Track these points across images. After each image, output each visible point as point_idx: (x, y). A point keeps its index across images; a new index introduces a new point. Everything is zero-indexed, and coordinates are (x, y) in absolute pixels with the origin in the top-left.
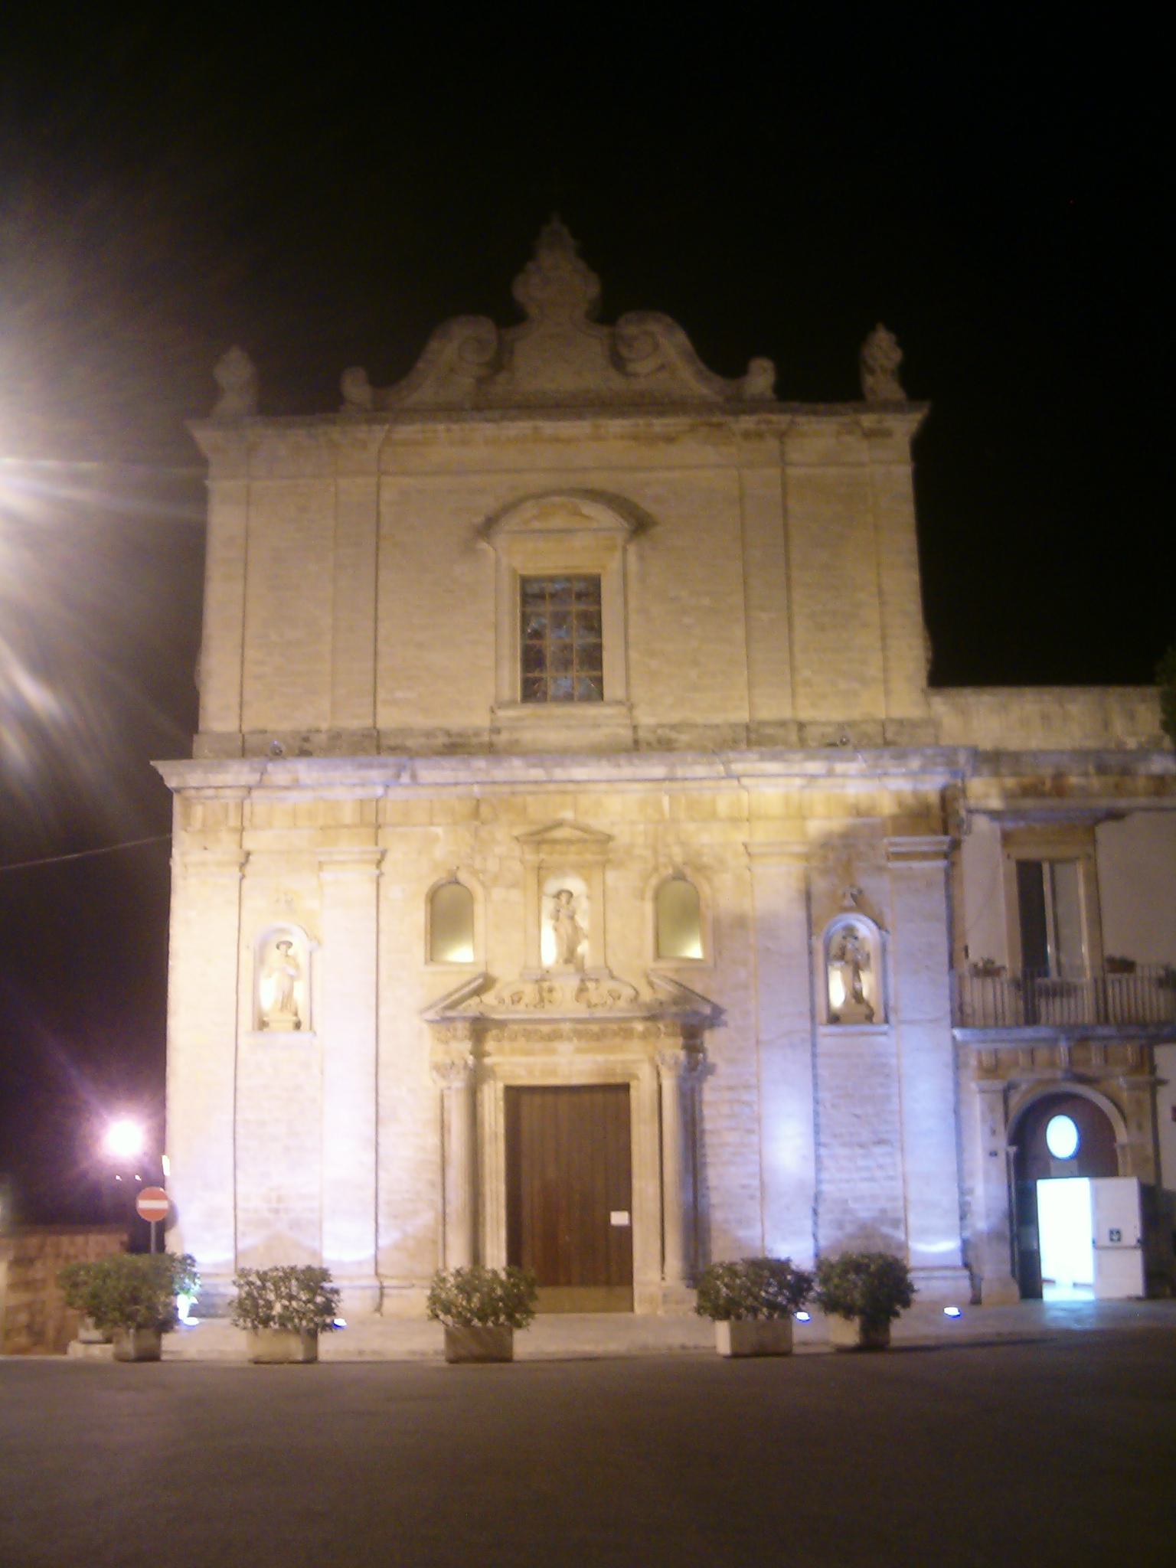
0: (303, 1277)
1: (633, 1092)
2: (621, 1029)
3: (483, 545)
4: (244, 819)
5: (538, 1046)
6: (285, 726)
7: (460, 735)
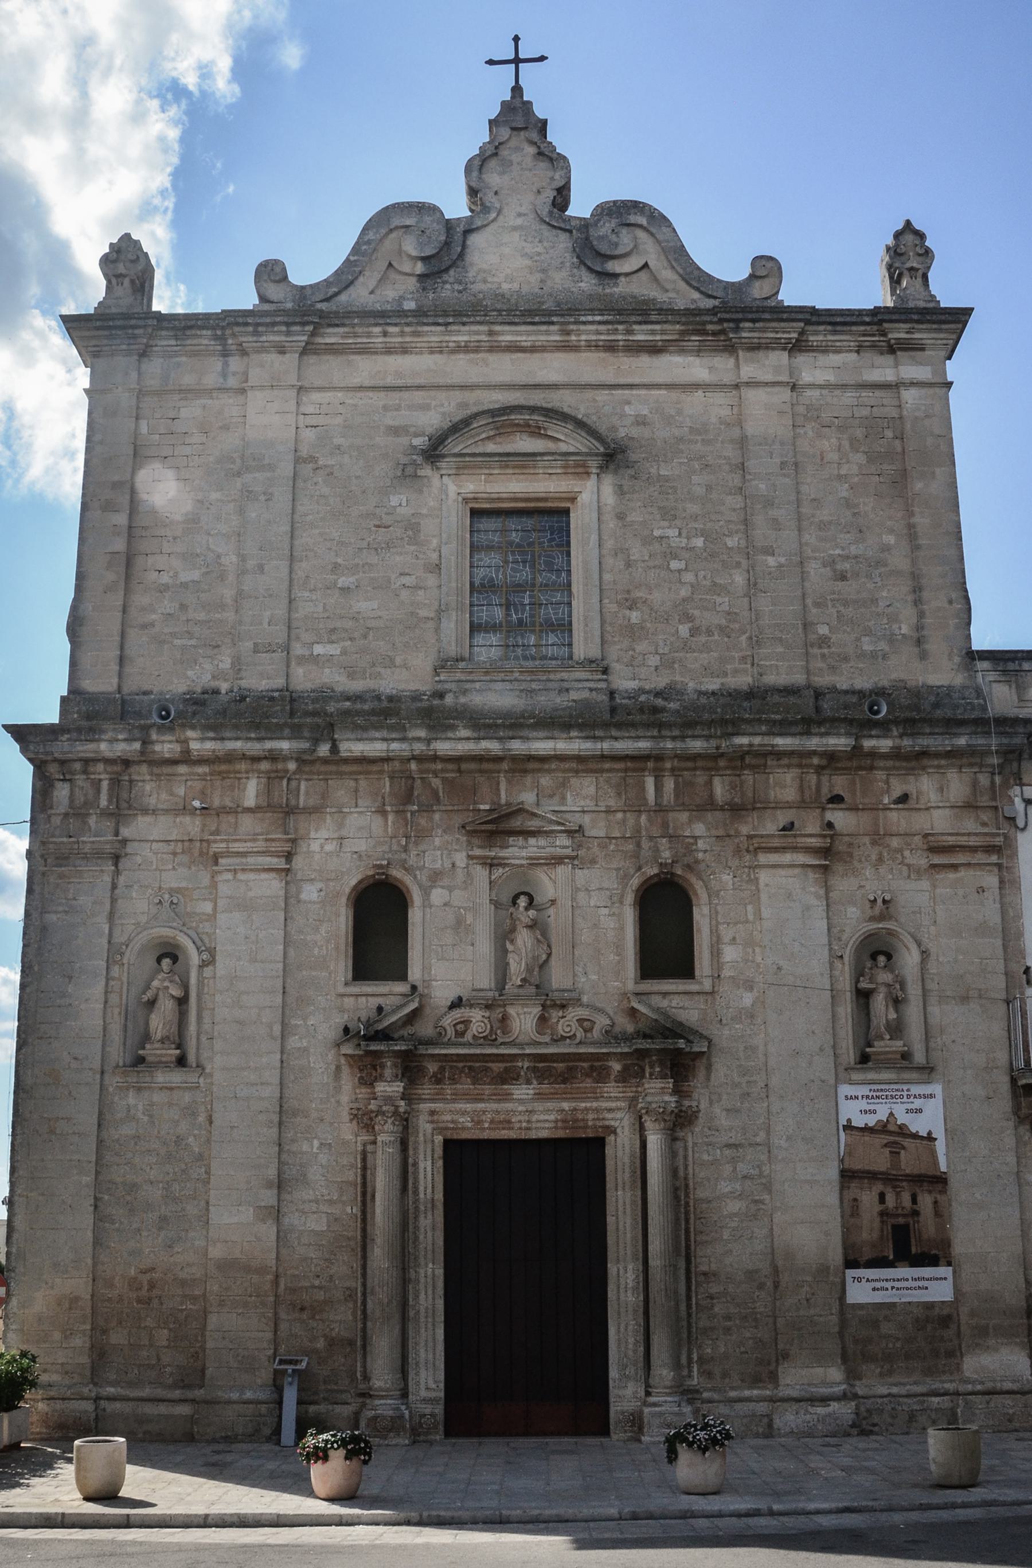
0: (717, 782)
1: (609, 1151)
2: (592, 1067)
3: (427, 471)
4: (580, 1516)
5: (488, 1089)
6: (179, 686)
7: (391, 699)
